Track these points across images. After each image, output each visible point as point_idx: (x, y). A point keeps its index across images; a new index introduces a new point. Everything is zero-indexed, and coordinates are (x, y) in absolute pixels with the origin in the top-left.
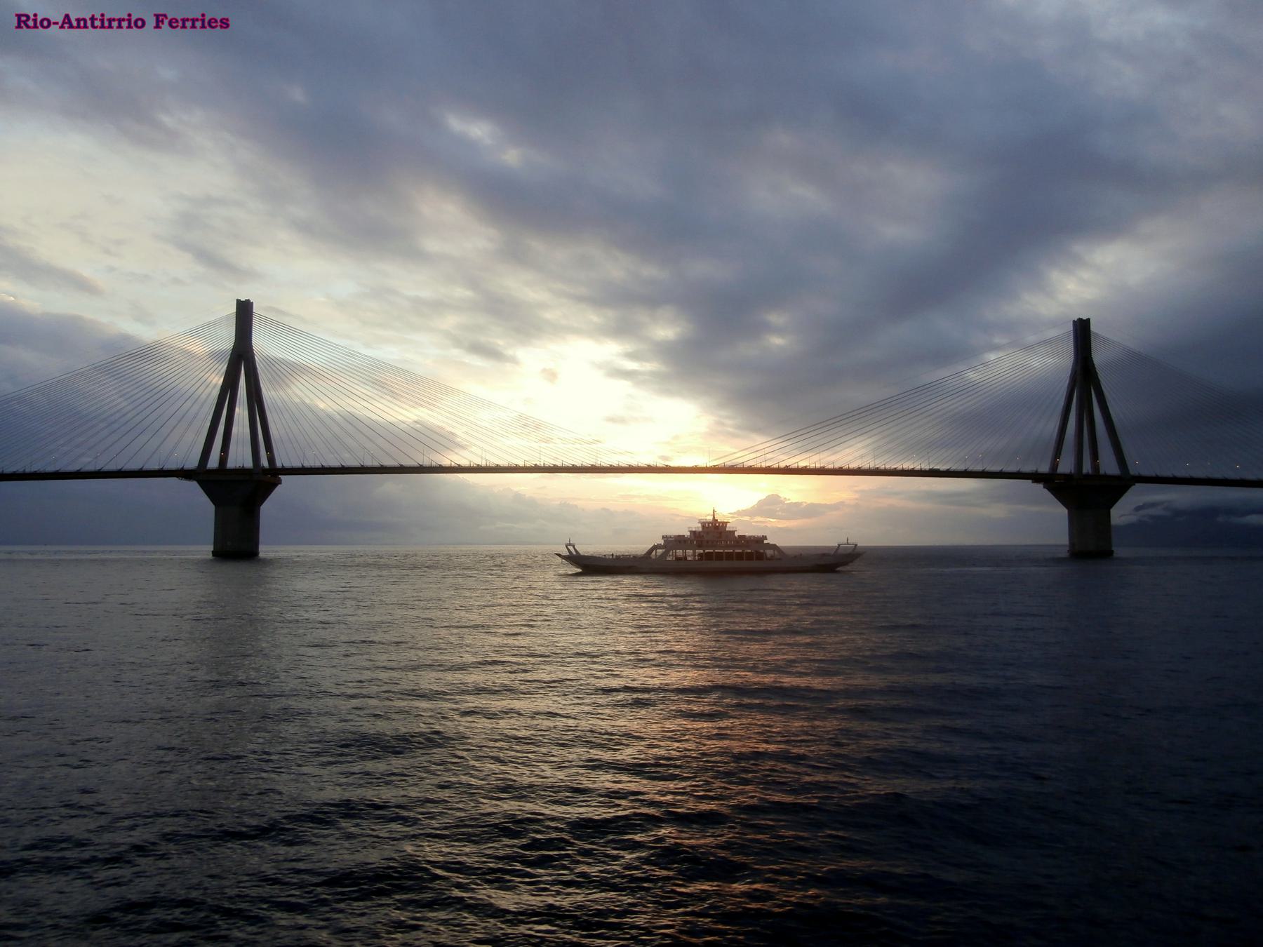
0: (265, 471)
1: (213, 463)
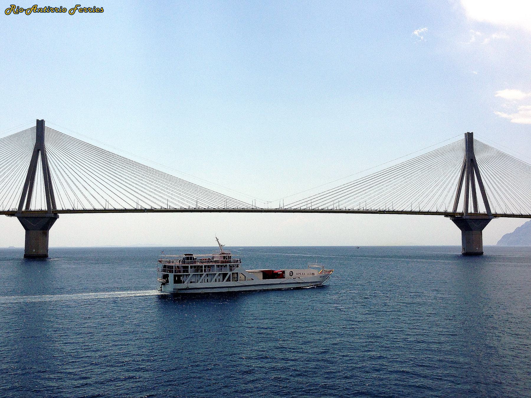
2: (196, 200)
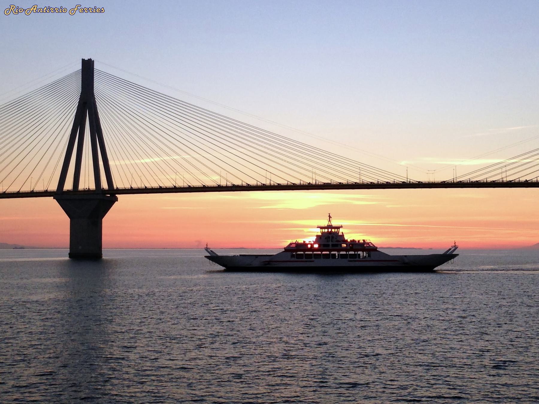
0: (104, 192)
1: (68, 186)
2: (358, 171)
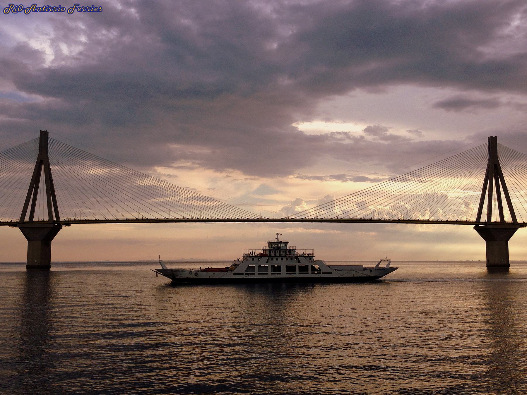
0: (54, 222)
1: (484, 219)
